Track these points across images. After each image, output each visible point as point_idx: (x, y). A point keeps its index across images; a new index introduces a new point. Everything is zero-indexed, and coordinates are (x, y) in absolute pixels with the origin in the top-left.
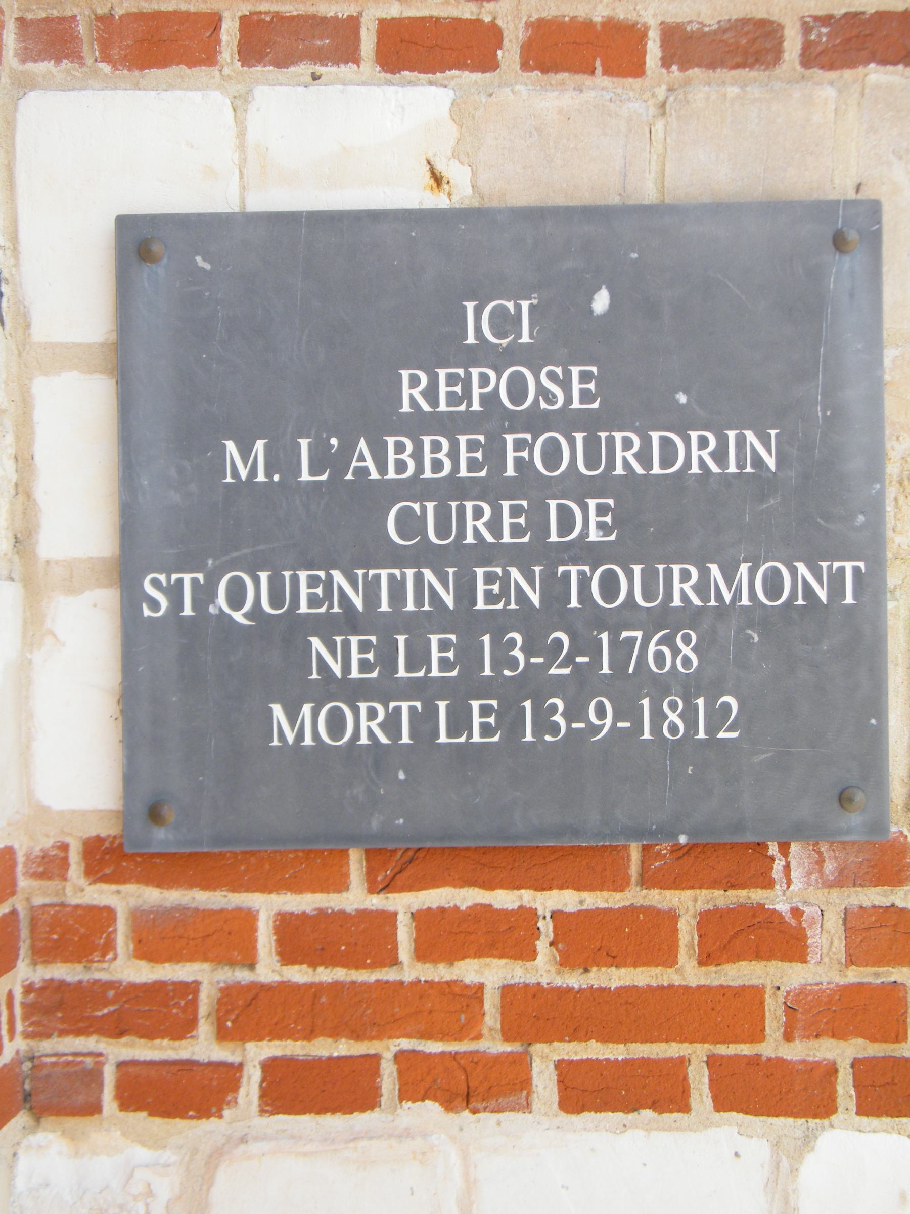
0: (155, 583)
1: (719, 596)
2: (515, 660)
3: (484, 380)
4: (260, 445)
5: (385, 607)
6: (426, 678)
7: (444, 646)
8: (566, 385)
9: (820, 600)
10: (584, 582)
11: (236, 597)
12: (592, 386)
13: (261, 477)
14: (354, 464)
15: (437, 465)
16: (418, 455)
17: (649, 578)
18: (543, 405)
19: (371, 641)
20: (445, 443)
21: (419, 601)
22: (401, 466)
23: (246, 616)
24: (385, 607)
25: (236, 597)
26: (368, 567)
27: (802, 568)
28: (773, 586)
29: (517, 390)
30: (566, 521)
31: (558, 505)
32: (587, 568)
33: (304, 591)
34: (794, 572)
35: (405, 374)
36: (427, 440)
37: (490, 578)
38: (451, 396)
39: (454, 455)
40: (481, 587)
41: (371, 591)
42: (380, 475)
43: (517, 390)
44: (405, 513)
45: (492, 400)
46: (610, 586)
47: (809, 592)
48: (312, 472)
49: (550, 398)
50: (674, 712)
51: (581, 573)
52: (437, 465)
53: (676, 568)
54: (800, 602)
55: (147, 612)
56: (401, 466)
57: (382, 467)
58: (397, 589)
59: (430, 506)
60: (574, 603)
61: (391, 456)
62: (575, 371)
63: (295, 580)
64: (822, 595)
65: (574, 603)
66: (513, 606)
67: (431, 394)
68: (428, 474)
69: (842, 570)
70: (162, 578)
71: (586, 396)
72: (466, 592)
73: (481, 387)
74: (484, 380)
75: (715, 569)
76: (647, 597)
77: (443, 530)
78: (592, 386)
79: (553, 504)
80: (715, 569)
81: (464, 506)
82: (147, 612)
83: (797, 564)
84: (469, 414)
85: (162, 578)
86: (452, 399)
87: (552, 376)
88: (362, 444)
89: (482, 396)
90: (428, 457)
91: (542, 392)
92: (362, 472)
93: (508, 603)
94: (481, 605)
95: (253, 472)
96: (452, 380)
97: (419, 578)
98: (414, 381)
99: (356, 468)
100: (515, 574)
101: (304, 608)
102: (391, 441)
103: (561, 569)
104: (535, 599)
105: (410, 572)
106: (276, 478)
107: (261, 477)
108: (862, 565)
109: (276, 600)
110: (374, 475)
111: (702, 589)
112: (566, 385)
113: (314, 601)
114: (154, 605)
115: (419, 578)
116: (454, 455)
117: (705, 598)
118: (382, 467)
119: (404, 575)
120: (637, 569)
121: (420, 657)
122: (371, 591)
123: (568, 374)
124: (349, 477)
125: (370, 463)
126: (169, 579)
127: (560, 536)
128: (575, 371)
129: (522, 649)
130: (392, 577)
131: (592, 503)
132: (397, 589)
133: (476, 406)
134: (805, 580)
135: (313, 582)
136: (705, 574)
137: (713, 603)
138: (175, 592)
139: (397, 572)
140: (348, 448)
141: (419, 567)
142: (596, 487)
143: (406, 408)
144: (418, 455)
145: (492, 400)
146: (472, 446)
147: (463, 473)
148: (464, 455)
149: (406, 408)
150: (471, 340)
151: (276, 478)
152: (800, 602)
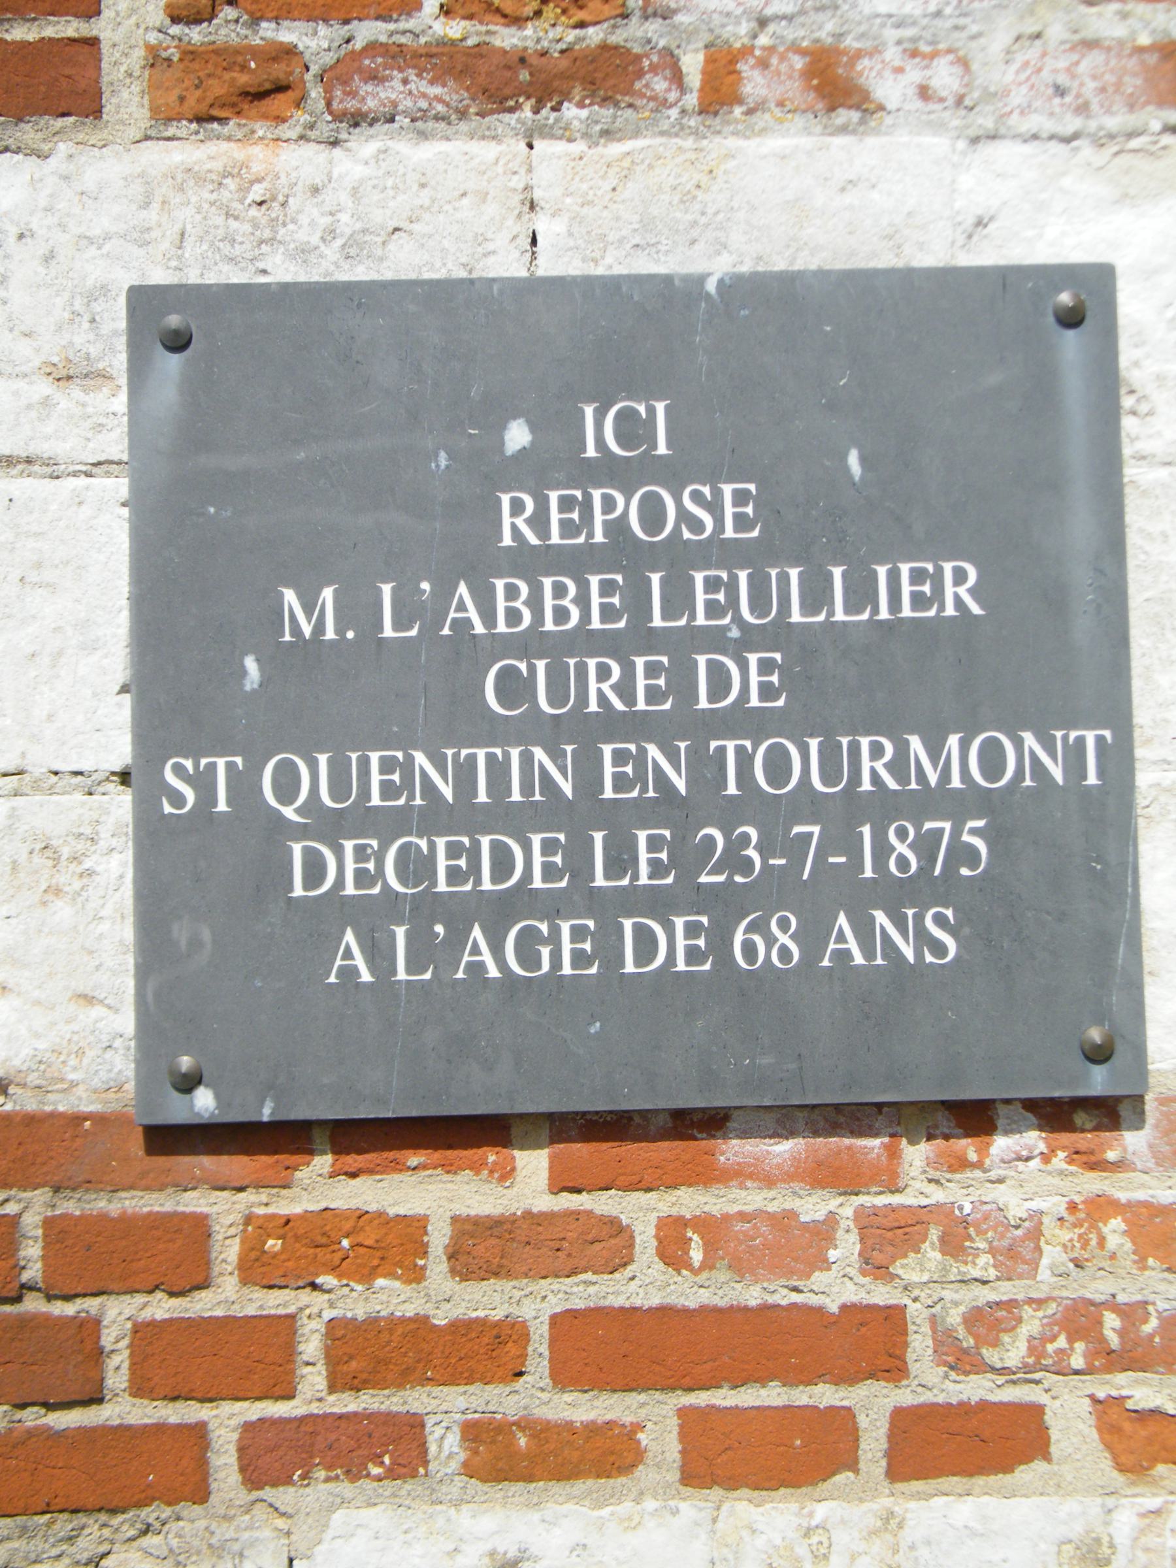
0: (179, 770)
1: (921, 776)
2: (749, 862)
3: (609, 504)
4: (328, 594)
5: (482, 797)
6: (632, 887)
7: (654, 844)
8: (714, 508)
9: (1053, 779)
10: (745, 760)
11: (287, 787)
12: (749, 510)
13: (330, 634)
14: (452, 614)
15: (561, 615)
16: (535, 601)
17: (830, 754)
18: (687, 535)
19: (664, 836)
20: (524, 589)
21: (527, 789)
22: (513, 616)
23: (298, 811)
24: (482, 797)
25: (287, 787)
26: (461, 745)
27: (1029, 739)
28: (992, 761)
29: (653, 515)
30: (719, 683)
31: (709, 662)
32: (748, 744)
33: (376, 778)
34: (1019, 744)
35: (505, 499)
36: (547, 583)
37: (620, 757)
38: (565, 525)
39: (583, 600)
40: (609, 770)
41: (465, 776)
42: (486, 628)
43: (653, 515)
44: (506, 675)
45: (618, 528)
46: (778, 767)
47: (1038, 768)
48: (397, 626)
49: (697, 525)
50: (785, 932)
51: (740, 750)
52: (561, 615)
53: (865, 742)
54: (1028, 782)
55: (168, 809)
56: (513, 616)
57: (489, 618)
58: (498, 771)
59: (541, 665)
60: (732, 789)
61: (501, 605)
62: (727, 489)
63: (364, 763)
64: (1057, 773)
65: (732, 789)
66: (418, 801)
67: (540, 522)
68: (549, 625)
69: (472, 758)
70: (188, 764)
71: (741, 522)
72: (589, 778)
73: (604, 512)
74: (609, 504)
75: (916, 743)
76: (826, 780)
77: (557, 695)
78: (749, 510)
79: (702, 660)
80: (916, 743)
81: (586, 664)
82: (168, 809)
83: (1024, 734)
84: (590, 547)
85: (188, 764)
86: (568, 528)
87: (697, 497)
88: (463, 589)
89: (605, 523)
90: (549, 603)
91: (683, 516)
92: (462, 625)
93: (644, 789)
94: (609, 793)
95: (319, 628)
96: (566, 504)
97: (527, 759)
98: (517, 507)
99: (454, 620)
100: (653, 752)
101: (376, 800)
102: (500, 584)
103: (714, 744)
104: (567, 788)
105: (515, 753)
106: (350, 635)
107: (330, 634)
108: (1107, 734)
109: (339, 788)
110: (479, 629)
111: (898, 767)
112: (714, 508)
113: (388, 790)
114: (178, 799)
115: (527, 759)
116: (583, 600)
117: (903, 779)
118: (489, 618)
119: (507, 756)
120: (323, 759)
121: (623, 858)
122: (465, 776)
123: (717, 493)
124: (446, 631)
125: (473, 614)
126: (196, 765)
127: (710, 701)
128: (727, 489)
129: (759, 848)
130: (490, 757)
131: (753, 659)
132: (498, 771)
133: (599, 537)
134: (1032, 753)
135: (387, 766)
136: (902, 749)
137: (913, 786)
138: (204, 783)
139: (498, 751)
140: (445, 592)
141: (854, 735)
142: (751, 639)
143: (507, 540)
144: (535, 601)
145: (618, 528)
146: (607, 588)
147: (596, 624)
148: (596, 600)
149: (507, 540)
150: (591, 452)
151: (350, 635)
152: (1028, 782)
